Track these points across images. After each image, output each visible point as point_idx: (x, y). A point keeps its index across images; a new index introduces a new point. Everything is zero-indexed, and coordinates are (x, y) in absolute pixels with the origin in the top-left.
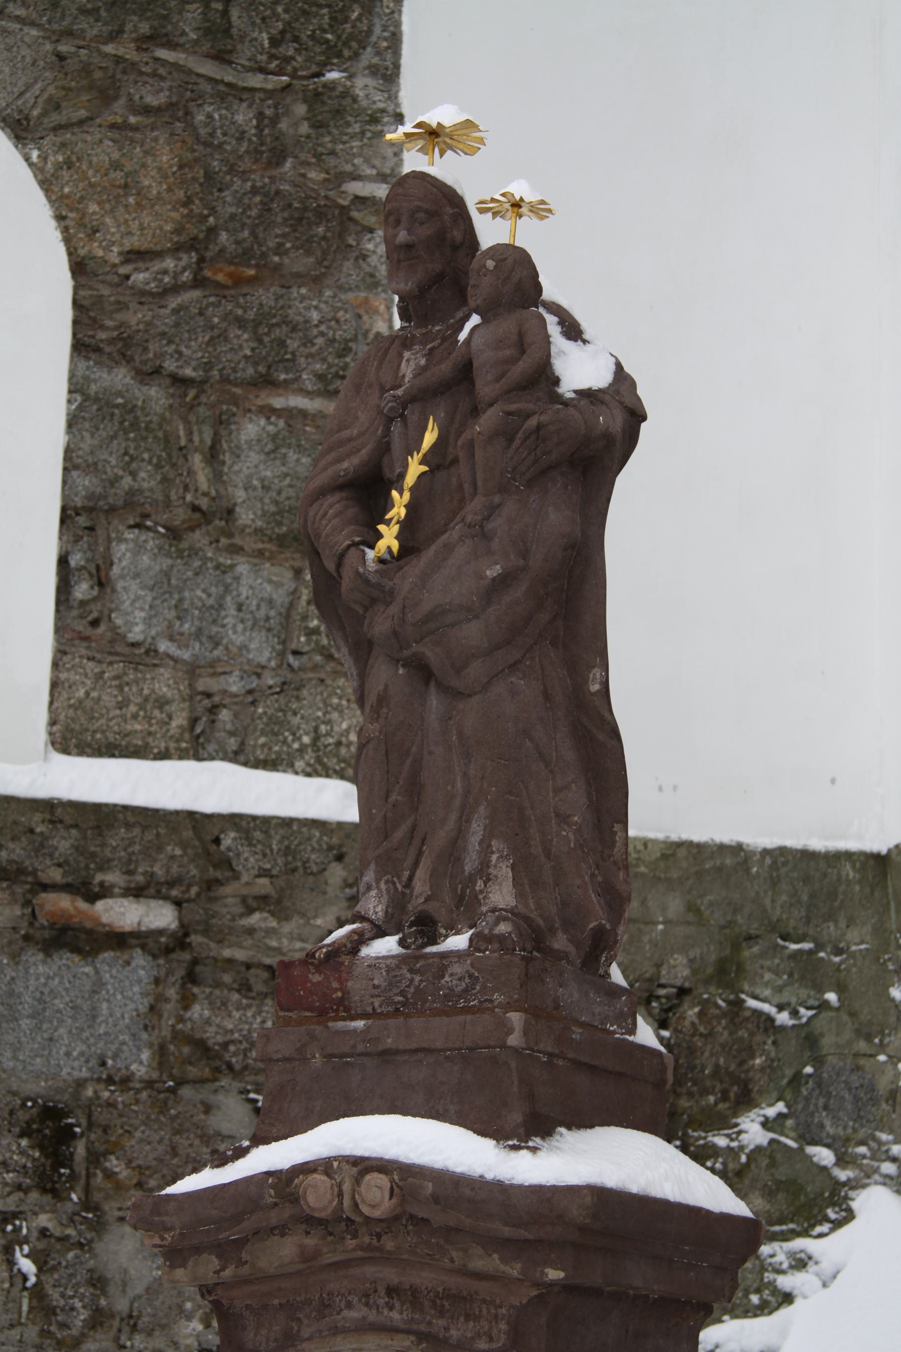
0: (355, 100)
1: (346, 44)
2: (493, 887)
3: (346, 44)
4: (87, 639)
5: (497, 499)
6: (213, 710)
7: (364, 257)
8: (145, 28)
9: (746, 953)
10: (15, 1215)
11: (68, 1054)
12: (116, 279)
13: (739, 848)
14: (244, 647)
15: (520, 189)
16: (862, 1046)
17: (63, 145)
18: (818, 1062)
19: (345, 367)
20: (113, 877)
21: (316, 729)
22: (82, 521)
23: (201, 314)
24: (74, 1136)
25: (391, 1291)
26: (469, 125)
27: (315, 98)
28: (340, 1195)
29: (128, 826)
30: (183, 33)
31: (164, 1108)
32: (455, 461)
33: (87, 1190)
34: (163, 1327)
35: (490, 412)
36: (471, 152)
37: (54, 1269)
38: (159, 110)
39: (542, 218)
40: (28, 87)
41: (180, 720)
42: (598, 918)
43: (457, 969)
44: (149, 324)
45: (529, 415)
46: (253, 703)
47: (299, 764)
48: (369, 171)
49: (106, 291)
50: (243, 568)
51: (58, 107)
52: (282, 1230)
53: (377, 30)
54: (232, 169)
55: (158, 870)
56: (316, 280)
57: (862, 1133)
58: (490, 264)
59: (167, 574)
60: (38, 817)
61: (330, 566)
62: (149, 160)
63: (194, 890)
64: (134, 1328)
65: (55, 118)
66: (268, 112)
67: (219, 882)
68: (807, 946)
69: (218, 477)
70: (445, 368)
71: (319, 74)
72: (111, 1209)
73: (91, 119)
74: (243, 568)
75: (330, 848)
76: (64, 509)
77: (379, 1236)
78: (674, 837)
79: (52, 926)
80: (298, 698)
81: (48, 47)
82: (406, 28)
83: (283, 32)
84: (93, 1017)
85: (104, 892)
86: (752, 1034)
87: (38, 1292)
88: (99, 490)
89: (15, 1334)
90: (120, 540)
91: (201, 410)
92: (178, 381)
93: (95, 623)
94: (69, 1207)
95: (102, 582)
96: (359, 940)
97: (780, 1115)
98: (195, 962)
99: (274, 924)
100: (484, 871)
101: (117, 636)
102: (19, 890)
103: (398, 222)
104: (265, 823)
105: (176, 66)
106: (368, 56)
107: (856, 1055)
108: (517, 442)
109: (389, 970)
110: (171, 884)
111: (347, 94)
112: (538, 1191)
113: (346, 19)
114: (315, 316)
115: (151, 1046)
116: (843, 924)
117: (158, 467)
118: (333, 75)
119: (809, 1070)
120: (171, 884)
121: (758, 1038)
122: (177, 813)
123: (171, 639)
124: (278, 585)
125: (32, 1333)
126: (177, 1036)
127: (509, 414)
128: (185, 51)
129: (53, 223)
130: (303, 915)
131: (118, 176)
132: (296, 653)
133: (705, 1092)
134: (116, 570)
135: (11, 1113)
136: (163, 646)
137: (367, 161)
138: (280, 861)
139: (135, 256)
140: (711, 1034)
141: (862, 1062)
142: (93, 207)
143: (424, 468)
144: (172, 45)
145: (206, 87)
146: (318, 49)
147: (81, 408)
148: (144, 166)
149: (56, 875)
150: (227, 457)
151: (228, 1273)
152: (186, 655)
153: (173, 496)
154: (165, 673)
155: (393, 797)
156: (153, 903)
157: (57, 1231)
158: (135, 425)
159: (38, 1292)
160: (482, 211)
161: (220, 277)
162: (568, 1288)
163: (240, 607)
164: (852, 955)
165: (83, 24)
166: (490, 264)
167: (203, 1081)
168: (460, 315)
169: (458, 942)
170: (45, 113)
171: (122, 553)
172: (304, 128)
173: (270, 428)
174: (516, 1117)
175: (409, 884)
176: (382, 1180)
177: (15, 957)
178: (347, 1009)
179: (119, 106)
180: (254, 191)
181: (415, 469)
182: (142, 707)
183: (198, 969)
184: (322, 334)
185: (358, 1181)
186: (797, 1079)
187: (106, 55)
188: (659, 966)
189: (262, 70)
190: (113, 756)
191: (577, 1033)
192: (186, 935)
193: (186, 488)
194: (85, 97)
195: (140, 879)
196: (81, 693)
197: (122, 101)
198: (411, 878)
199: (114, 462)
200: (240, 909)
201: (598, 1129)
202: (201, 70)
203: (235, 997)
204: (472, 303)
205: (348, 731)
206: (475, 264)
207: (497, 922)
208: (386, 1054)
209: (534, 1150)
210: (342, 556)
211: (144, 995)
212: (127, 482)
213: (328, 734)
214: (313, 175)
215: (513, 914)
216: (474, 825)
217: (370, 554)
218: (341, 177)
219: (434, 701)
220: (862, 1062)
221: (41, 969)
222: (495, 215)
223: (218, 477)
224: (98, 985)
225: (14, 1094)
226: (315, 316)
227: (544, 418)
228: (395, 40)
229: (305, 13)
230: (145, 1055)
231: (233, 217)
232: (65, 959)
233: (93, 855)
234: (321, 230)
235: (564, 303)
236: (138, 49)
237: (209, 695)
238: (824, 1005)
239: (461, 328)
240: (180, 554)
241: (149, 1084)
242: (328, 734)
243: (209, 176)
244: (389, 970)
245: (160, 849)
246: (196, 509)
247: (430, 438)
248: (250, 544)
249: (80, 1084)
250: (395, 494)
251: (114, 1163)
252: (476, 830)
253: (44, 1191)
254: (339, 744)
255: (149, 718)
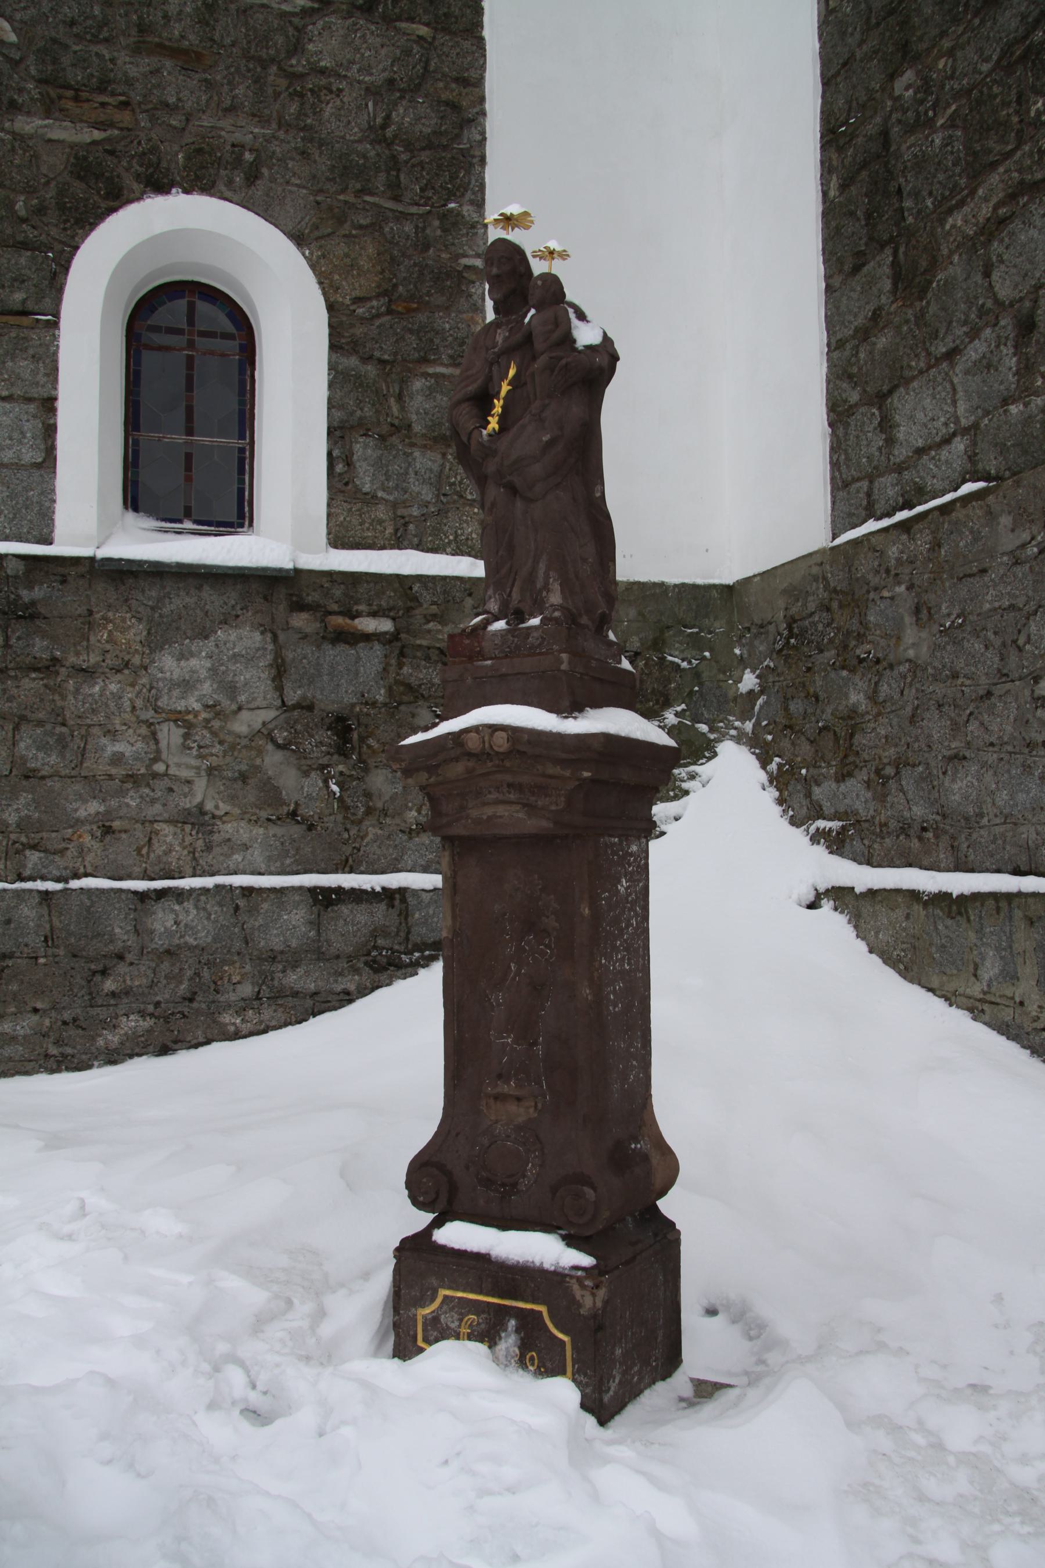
0: (463, 217)
1: (457, 189)
2: (551, 595)
3: (457, 189)
4: (343, 492)
5: (547, 401)
6: (406, 524)
7: (471, 296)
8: (358, 186)
9: (667, 635)
10: (328, 766)
11: (346, 692)
12: (349, 312)
13: (662, 584)
14: (419, 493)
15: (553, 245)
16: (721, 676)
17: (321, 247)
18: (701, 684)
19: (463, 351)
20: (362, 607)
21: (456, 532)
22: (338, 433)
23: (391, 327)
24: (352, 729)
25: (510, 785)
26: (526, 214)
27: (443, 217)
28: (484, 742)
29: (368, 582)
30: (377, 188)
31: (393, 715)
32: (525, 384)
33: (360, 754)
34: (399, 814)
35: (542, 358)
36: (527, 228)
37: (347, 789)
38: (366, 227)
39: (564, 259)
40: (302, 219)
41: (390, 530)
42: (603, 608)
43: (535, 634)
44: (365, 334)
45: (561, 358)
46: (425, 520)
47: (449, 550)
48: (471, 253)
49: (344, 319)
50: (417, 454)
51: (317, 228)
52: (457, 759)
53: (473, 182)
54: (404, 255)
55: (384, 603)
56: (447, 308)
57: (721, 717)
58: (539, 283)
59: (380, 458)
60: (324, 580)
61: (465, 439)
62: (363, 252)
63: (401, 613)
64: (386, 815)
65: (317, 234)
66: (420, 225)
67: (413, 608)
68: (695, 630)
69: (403, 409)
70: (518, 337)
71: (445, 205)
72: (371, 762)
73: (334, 233)
74: (417, 454)
75: (465, 590)
76: (329, 428)
77: (503, 760)
78: (632, 580)
79: (335, 631)
80: (447, 518)
81: (312, 198)
82: (487, 180)
83: (426, 185)
84: (357, 673)
85: (358, 615)
86: (670, 673)
87: (341, 800)
88: (345, 418)
89: (332, 818)
90: (357, 442)
91: (393, 376)
92: (382, 362)
93: (347, 484)
94: (352, 762)
95: (349, 463)
96: (487, 623)
97: (683, 710)
98: (403, 647)
99: (440, 627)
100: (546, 587)
101: (358, 490)
102: (318, 615)
103: (492, 264)
104: (433, 579)
105: (374, 204)
106: (469, 195)
107: (719, 681)
108: (556, 372)
109: (502, 636)
110: (390, 610)
111: (459, 214)
112: (578, 737)
113: (457, 177)
114: (447, 326)
115: (385, 687)
116: (712, 619)
117: (373, 405)
118: (452, 205)
119: (696, 688)
120: (390, 610)
121: (673, 674)
122: (391, 575)
123: (384, 491)
124: (434, 461)
125: (340, 818)
126: (397, 682)
127: (551, 358)
128: (379, 196)
129: (317, 286)
130: (454, 623)
131: (348, 261)
132: (444, 495)
133: (649, 701)
134: (355, 457)
135: (322, 719)
136: (380, 494)
137: (470, 247)
138: (442, 597)
139: (357, 300)
140: (650, 673)
141: (721, 684)
142: (336, 277)
143: (510, 388)
144: (372, 194)
145: (390, 214)
146: (444, 193)
147: (334, 377)
148: (361, 255)
149: (335, 607)
150: (407, 399)
151: (432, 780)
152: (391, 498)
153: (381, 419)
154: (382, 507)
155: (500, 553)
156: (382, 619)
157: (348, 773)
158: (361, 385)
159: (341, 800)
160: (534, 257)
161: (400, 309)
162: (592, 781)
163: (416, 474)
164: (717, 634)
165: (328, 186)
166: (539, 283)
167: (410, 703)
168: (524, 310)
169: (535, 621)
170: (311, 232)
171: (357, 448)
172: (439, 232)
173: (428, 383)
174: (566, 703)
175: (510, 595)
176: (504, 734)
177: (319, 647)
178: (483, 656)
179: (347, 226)
180: (415, 265)
181: (505, 388)
182: (371, 524)
183: (405, 650)
184: (451, 335)
185: (492, 735)
186: (691, 693)
187: (340, 201)
188: (625, 642)
189: (417, 204)
190: (358, 549)
191: (594, 664)
192: (399, 634)
193: (387, 415)
194: (330, 222)
195: (375, 608)
196: (342, 519)
197: (349, 223)
198: (511, 592)
199: (351, 403)
200: (423, 621)
201: (605, 709)
202: (386, 205)
203: (423, 663)
204: (531, 303)
205: (471, 533)
206: (532, 283)
207: (554, 611)
208: (503, 676)
209: (575, 718)
210: (471, 433)
211: (380, 663)
212: (359, 413)
213: (462, 534)
214: (443, 255)
215: (562, 608)
216: (541, 565)
217: (485, 432)
218: (457, 257)
219: (519, 504)
220: (721, 684)
221: (331, 652)
222: (541, 258)
223: (403, 409)
224: (358, 659)
225: (323, 711)
226: (447, 326)
227: (569, 360)
228: (482, 187)
229: (437, 175)
230: (382, 691)
231: (405, 279)
232: (342, 647)
233: (352, 597)
234: (449, 283)
235: (576, 302)
236: (355, 196)
237: (403, 517)
238: (704, 658)
239: (526, 316)
240: (386, 448)
241: (385, 705)
242: (462, 534)
243: (393, 259)
244: (502, 636)
245: (384, 593)
246: (392, 425)
247: (512, 372)
248: (420, 442)
249: (353, 705)
250: (496, 401)
251: (371, 741)
252: (542, 566)
253: (340, 755)
254: (467, 539)
255: (375, 530)
